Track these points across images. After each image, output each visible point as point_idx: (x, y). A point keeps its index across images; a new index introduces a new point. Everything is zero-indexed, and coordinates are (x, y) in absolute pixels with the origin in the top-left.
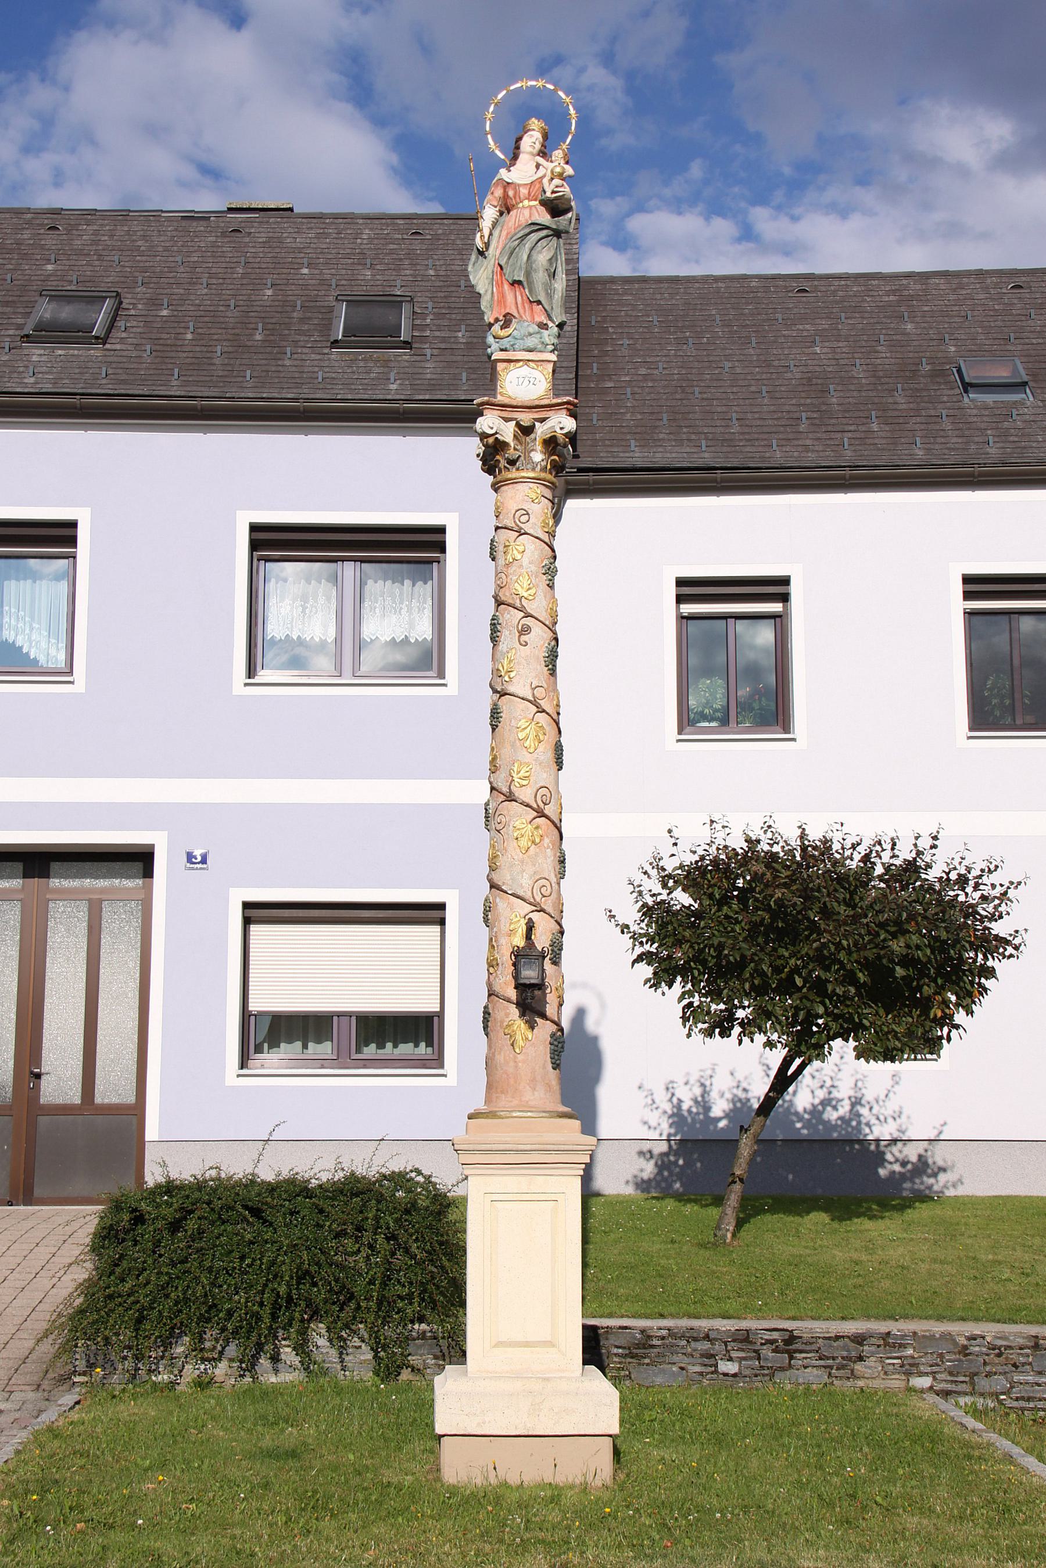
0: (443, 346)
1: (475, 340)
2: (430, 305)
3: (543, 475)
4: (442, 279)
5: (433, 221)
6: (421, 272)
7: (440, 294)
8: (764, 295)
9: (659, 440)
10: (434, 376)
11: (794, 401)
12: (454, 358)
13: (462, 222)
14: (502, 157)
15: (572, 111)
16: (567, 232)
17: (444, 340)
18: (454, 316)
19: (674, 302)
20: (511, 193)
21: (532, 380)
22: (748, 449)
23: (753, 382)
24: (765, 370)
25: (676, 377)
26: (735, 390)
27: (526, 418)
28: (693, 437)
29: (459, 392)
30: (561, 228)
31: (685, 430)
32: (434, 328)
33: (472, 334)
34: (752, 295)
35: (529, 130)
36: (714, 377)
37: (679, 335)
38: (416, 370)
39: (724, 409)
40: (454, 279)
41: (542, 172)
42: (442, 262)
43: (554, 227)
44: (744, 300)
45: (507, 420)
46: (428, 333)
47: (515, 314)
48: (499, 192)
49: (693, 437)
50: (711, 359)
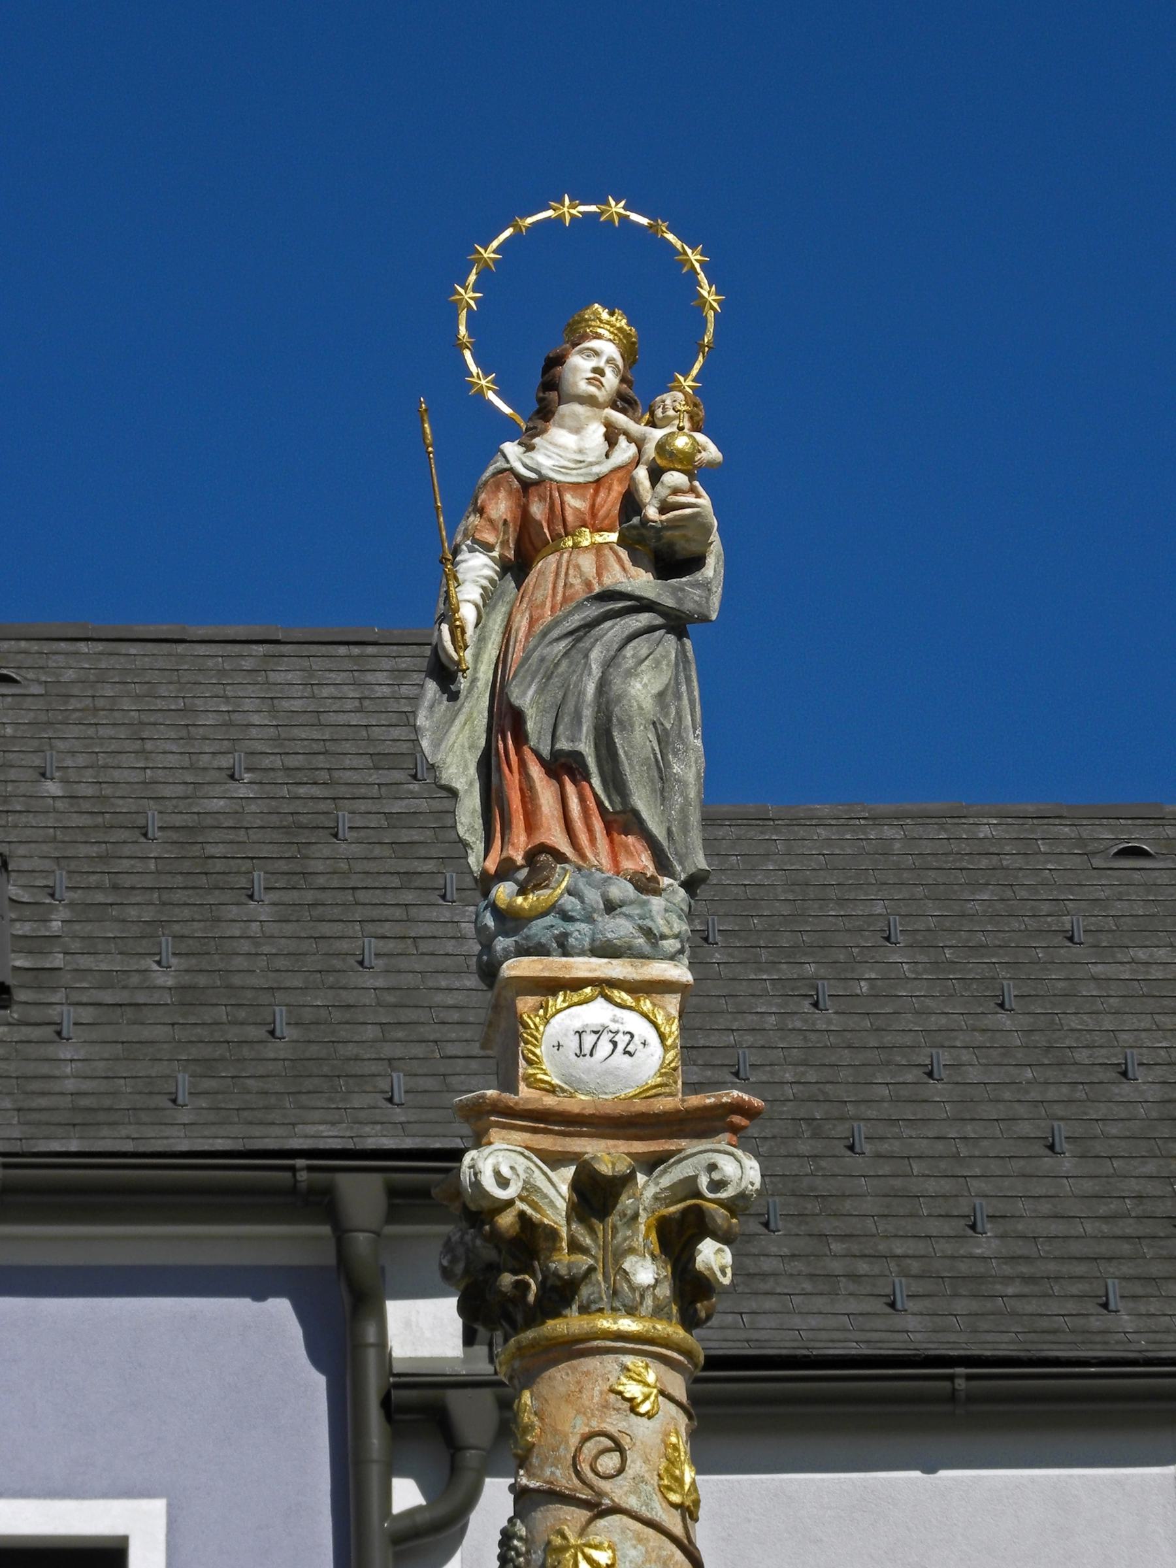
0: (108, 997)
1: (202, 980)
2: (61, 879)
3: (662, 1328)
4: (86, 806)
5: (47, 647)
6: (23, 788)
7: (84, 850)
8: (1019, 862)
9: (764, 1276)
10: (87, 1085)
11: (1150, 1168)
12: (146, 1033)
13: (133, 649)
14: (506, 410)
15: (706, 291)
16: (704, 619)
17: (108, 980)
18: (133, 913)
19: (759, 878)
20: (538, 510)
21: (622, 1040)
22: (1031, 1307)
23: (1021, 1110)
24: (1052, 1074)
25: (789, 1091)
26: (969, 1130)
27: (609, 1155)
28: (863, 1267)
29: (168, 1131)
30: (689, 606)
31: (836, 1247)
32: (75, 946)
33: (193, 962)
34: (984, 863)
35: (585, 337)
36: (905, 1092)
37: (786, 971)
38: (31, 1068)
39: (946, 1186)
40: (123, 806)
41: (625, 451)
42: (81, 760)
43: (670, 602)
44: (962, 878)
45: (554, 1160)
46: (58, 960)
47: (565, 848)
48: (501, 507)
49: (863, 1267)
50: (888, 1039)
